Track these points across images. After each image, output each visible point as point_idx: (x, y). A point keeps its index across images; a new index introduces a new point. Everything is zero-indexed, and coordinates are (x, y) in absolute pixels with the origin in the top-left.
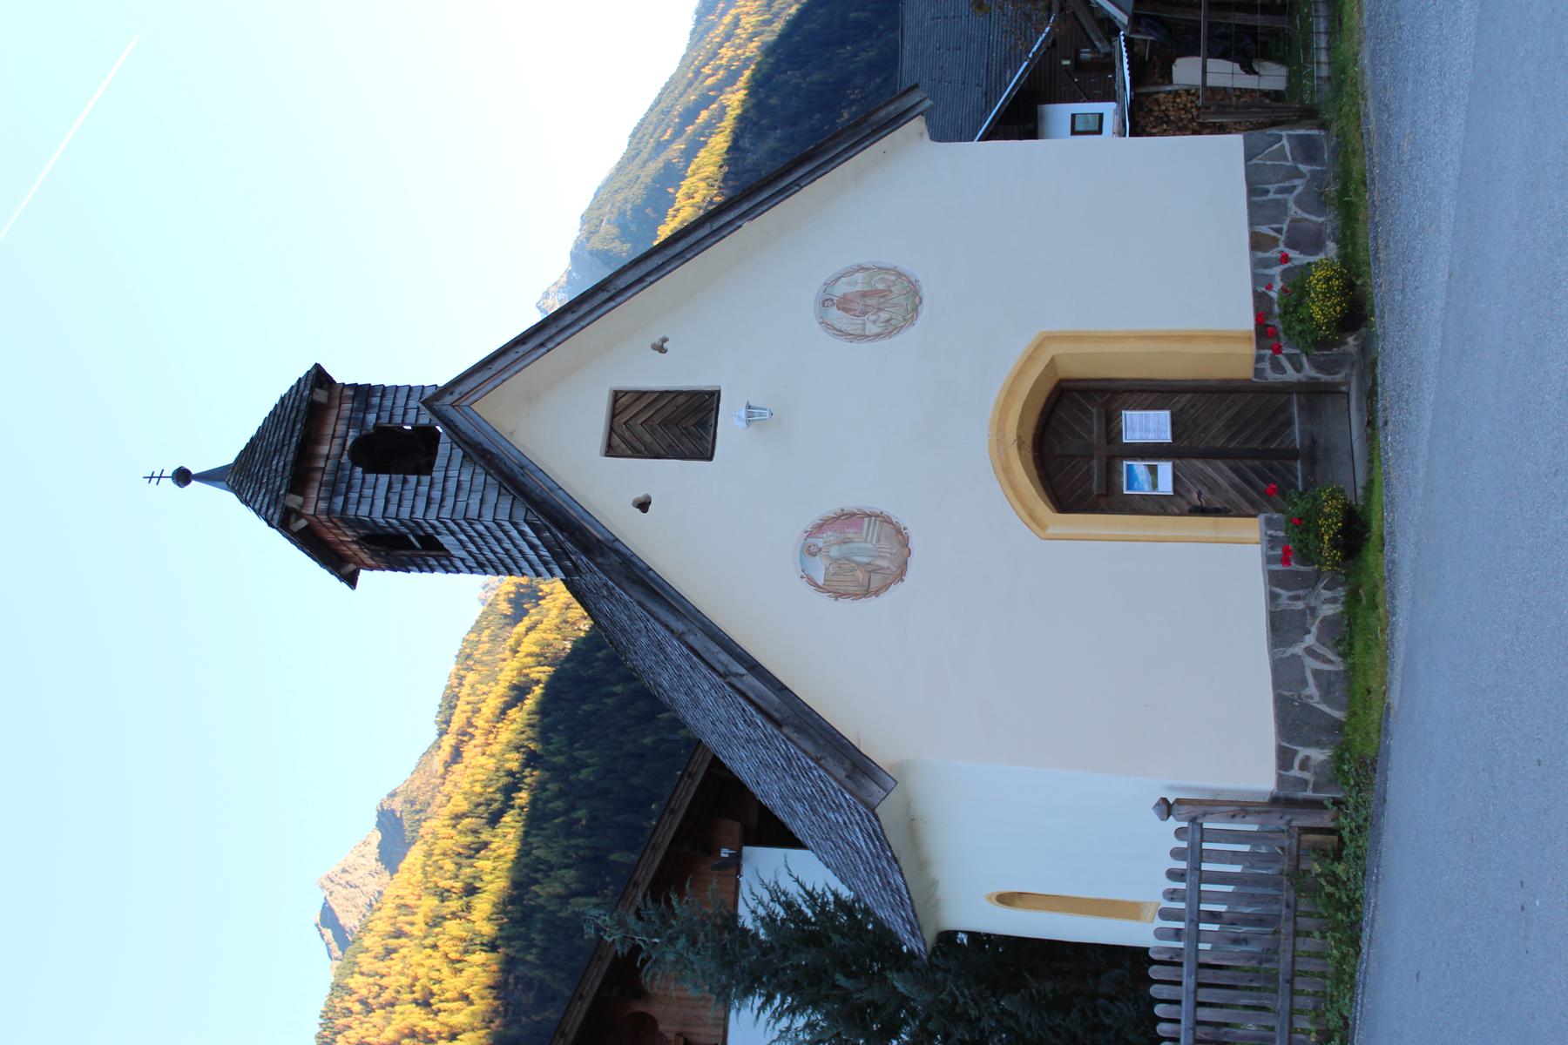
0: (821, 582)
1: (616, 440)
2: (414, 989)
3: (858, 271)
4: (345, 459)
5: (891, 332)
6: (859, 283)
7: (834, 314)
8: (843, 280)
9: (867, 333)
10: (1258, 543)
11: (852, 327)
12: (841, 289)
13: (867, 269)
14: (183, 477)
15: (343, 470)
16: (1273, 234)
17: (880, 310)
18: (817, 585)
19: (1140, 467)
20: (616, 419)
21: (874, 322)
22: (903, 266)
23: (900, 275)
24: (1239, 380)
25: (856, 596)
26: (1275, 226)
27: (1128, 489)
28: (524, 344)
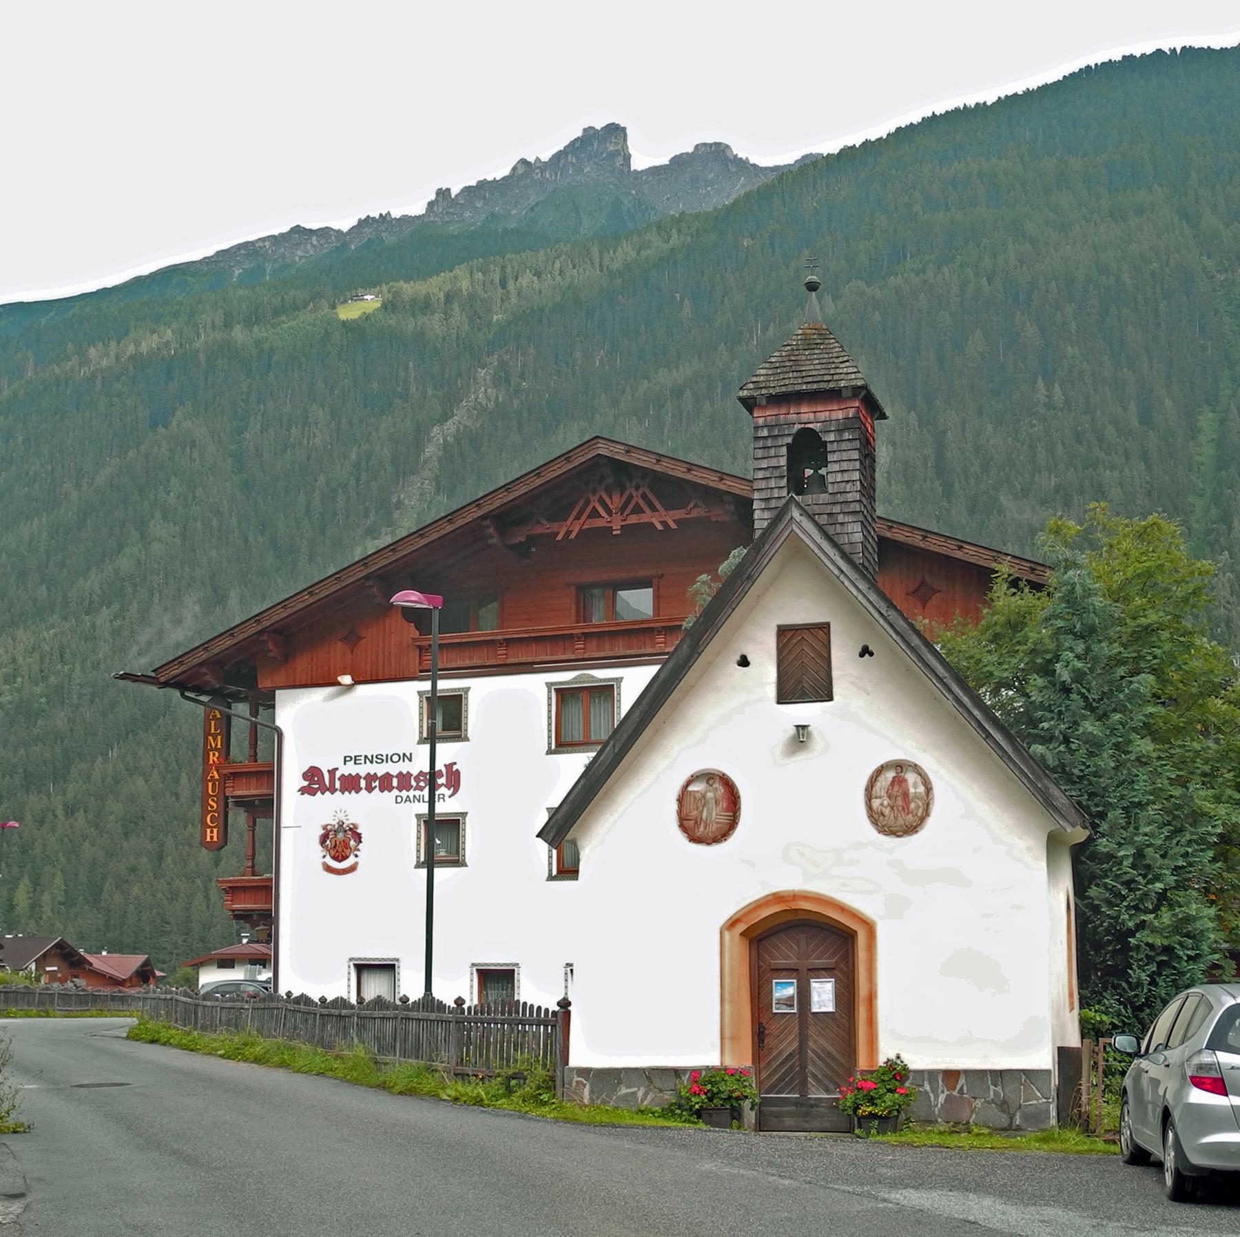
0: (690, 788)
1: (789, 635)
4: (798, 427)
5: (872, 817)
7: (890, 775)
8: (919, 779)
9: (873, 800)
10: (722, 1064)
12: (911, 777)
13: (928, 796)
15: (788, 428)
16: (958, 1087)
17: (892, 808)
19: (791, 991)
20: (806, 631)
24: (206, 968)
25: (680, 812)
26: (965, 1089)
27: (776, 983)
28: (842, 558)
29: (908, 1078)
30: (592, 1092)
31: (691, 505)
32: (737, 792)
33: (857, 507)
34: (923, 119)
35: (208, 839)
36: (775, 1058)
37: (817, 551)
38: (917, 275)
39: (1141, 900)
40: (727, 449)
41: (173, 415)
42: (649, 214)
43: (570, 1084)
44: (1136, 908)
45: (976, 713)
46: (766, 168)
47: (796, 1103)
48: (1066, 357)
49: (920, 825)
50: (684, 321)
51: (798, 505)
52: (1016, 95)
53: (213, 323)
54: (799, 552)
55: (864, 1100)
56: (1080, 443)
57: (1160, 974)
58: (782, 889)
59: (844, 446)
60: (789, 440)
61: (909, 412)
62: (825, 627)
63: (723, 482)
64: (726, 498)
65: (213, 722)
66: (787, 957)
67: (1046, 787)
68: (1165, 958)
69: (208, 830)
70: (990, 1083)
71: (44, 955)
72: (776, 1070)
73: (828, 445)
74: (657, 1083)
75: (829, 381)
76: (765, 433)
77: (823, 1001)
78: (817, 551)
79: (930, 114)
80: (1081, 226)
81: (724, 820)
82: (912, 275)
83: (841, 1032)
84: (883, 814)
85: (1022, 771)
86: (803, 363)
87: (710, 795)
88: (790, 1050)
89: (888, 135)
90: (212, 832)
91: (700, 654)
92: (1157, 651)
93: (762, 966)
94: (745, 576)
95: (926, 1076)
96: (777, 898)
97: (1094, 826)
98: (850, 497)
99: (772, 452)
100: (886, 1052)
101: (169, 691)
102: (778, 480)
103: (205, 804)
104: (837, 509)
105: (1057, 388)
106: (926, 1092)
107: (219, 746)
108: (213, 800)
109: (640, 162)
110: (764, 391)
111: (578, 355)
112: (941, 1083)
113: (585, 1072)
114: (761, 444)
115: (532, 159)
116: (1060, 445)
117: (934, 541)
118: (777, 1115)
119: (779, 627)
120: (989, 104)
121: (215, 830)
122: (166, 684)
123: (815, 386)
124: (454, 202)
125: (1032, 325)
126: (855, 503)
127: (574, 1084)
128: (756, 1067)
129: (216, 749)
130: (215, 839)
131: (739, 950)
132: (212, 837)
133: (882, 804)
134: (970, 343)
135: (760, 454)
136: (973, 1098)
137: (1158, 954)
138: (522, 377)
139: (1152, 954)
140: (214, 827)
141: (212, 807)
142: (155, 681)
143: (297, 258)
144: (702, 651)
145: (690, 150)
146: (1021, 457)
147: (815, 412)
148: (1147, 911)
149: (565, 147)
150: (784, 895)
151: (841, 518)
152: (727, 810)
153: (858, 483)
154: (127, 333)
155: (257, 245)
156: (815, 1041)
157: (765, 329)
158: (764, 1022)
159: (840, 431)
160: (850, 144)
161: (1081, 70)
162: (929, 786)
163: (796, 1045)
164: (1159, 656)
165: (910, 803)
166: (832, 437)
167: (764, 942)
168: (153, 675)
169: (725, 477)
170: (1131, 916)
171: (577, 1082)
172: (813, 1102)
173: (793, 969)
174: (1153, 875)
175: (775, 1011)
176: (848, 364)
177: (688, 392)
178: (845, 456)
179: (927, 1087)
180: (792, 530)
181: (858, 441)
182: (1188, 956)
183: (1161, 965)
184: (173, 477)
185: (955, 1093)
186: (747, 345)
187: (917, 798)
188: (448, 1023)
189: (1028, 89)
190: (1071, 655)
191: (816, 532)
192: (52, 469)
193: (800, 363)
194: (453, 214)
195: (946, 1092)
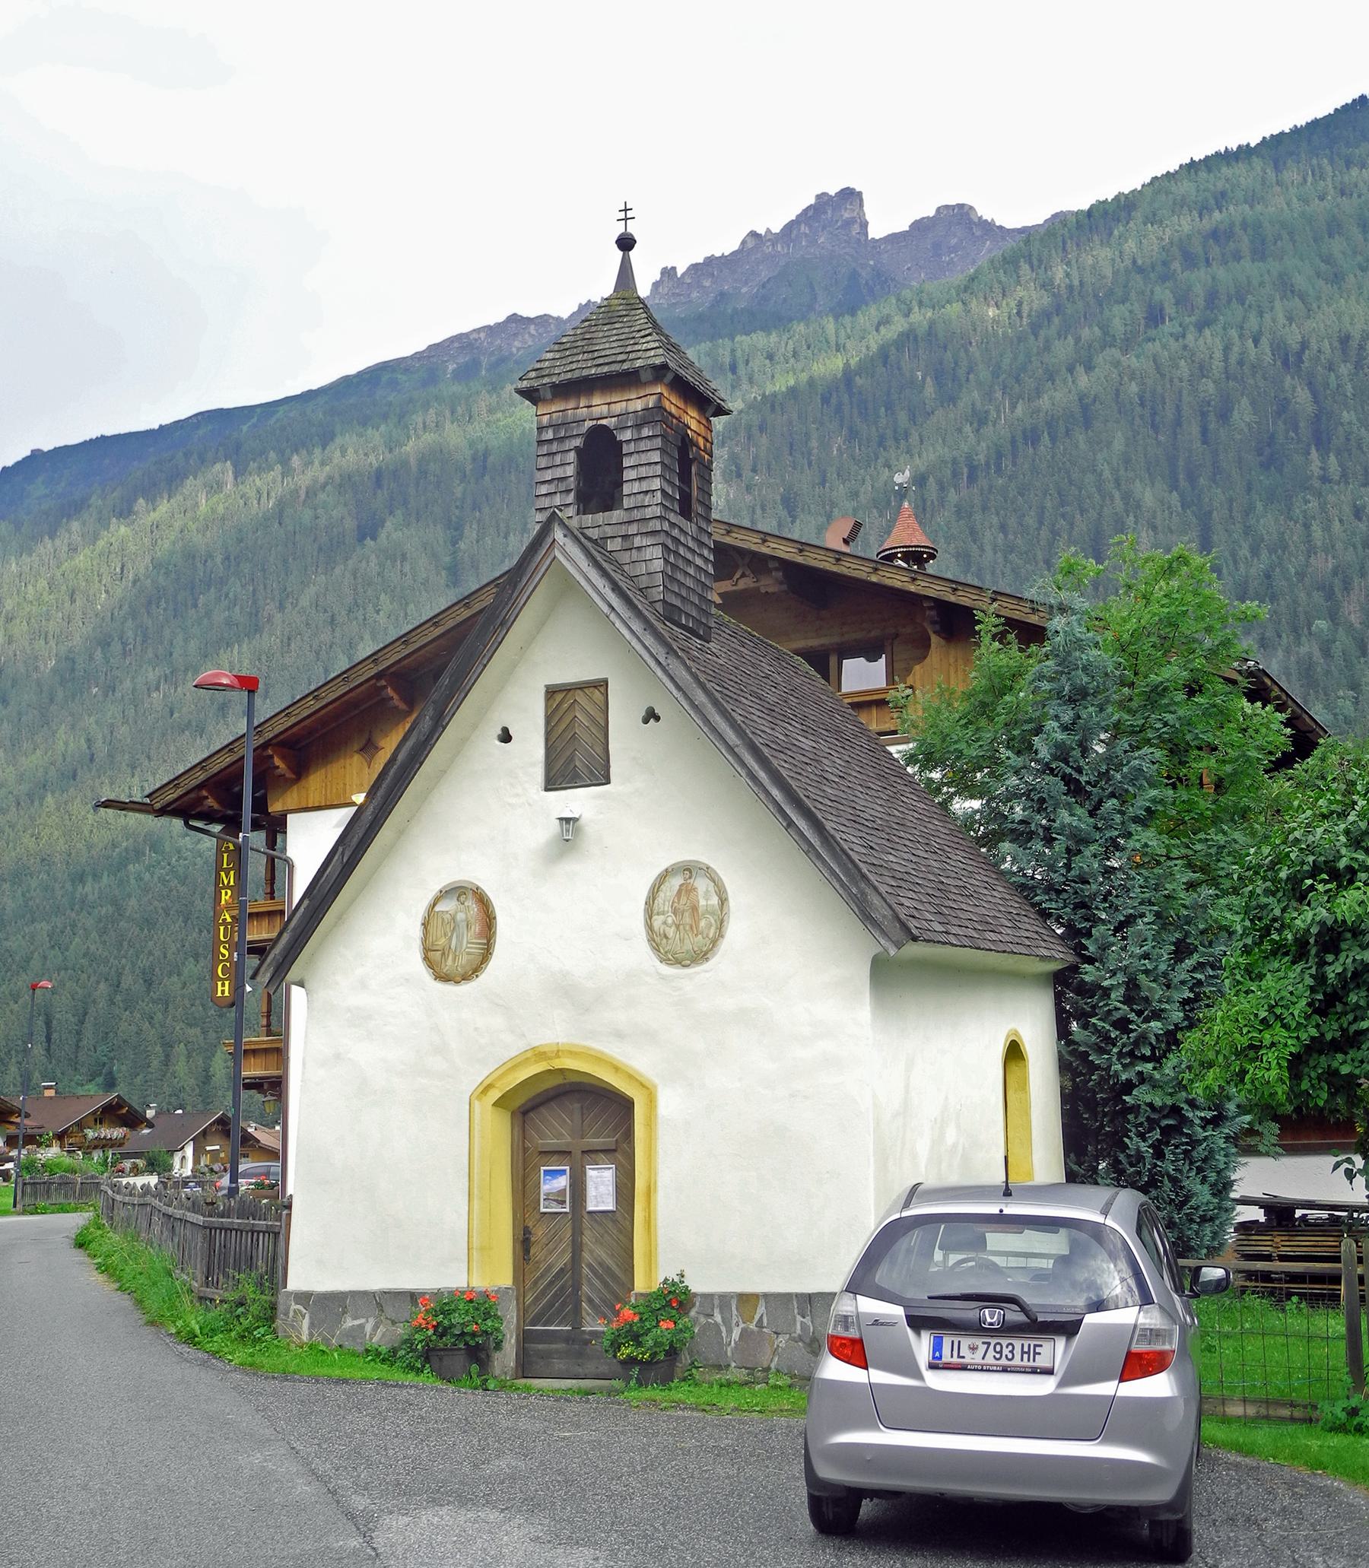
0: (437, 909)
1: (559, 697)
2: (1080, 369)
3: (720, 898)
4: (588, 424)
6: (707, 899)
7: (676, 882)
9: (654, 917)
11: (661, 901)
12: (702, 884)
14: (626, 243)
16: (757, 1317)
17: (678, 927)
18: (434, 905)
19: (562, 1182)
21: (665, 923)
22: (724, 945)
23: (714, 943)
28: (613, 590)
29: (694, 1305)
30: (312, 1325)
31: (737, 575)
32: (493, 911)
33: (656, 525)
34: (1181, 166)
35: (219, 994)
36: (542, 1276)
37: (583, 583)
38: (1177, 340)
39: (1136, 1043)
40: (975, 541)
41: (383, 527)
42: (889, 286)
43: (286, 1314)
44: (1131, 1054)
45: (776, 793)
46: (1013, 230)
47: (567, 1338)
48: (1342, 424)
49: (711, 949)
50: (927, 401)
51: (562, 523)
52: (1282, 134)
53: (424, 423)
54: (568, 586)
55: (626, 1337)
56: (1360, 520)
57: (1167, 1144)
58: (543, 1042)
59: (643, 446)
60: (578, 442)
61: (1171, 492)
62: (602, 685)
63: (766, 544)
64: (772, 565)
65: (225, 855)
66: (559, 1136)
67: (863, 893)
68: (1171, 1122)
69: (220, 983)
70: (796, 1311)
71: (204, 1133)
72: (543, 1293)
73: (624, 445)
74: (389, 1311)
75: (623, 361)
76: (549, 435)
77: (601, 1196)
78: (583, 583)
79: (1188, 161)
80: (1355, 276)
81: (476, 950)
82: (1172, 340)
83: (621, 1237)
84: (666, 937)
85: (833, 872)
86: (598, 341)
87: (460, 916)
88: (560, 1265)
89: (1143, 186)
90: (223, 985)
91: (444, 728)
92: (1168, 717)
93: (529, 1148)
94: (499, 621)
95: (716, 1302)
96: (539, 1054)
97: (1079, 949)
98: (649, 513)
99: (558, 459)
100: (665, 1271)
101: (164, 820)
102: (564, 495)
103: (216, 952)
104: (633, 529)
105: (1332, 458)
106: (716, 1324)
107: (232, 883)
108: (224, 947)
109: (877, 230)
110: (546, 380)
111: (814, 443)
112: (735, 1312)
113: (304, 1297)
114: (545, 449)
115: (762, 231)
116: (1337, 522)
117: (1005, 605)
118: (546, 1356)
119: (547, 687)
120: (1253, 145)
121: (227, 983)
122: (162, 812)
123: (606, 369)
124: (680, 281)
125: (1302, 389)
126: (654, 521)
127: (291, 1314)
128: (518, 1290)
129: (228, 887)
130: (227, 994)
131: (497, 1130)
132: (223, 992)
133: (665, 923)
134: (1236, 412)
135: (543, 462)
136: (775, 1333)
137: (1165, 1117)
138: (754, 470)
139: (1155, 1116)
140: (226, 979)
141: (224, 955)
142: (149, 808)
143: (514, 350)
144: (447, 724)
145: (931, 213)
146: (1295, 538)
147: (609, 404)
148: (1145, 1059)
149: (798, 216)
150: (546, 1049)
151: (638, 541)
152: (480, 935)
153: (659, 493)
154: (332, 439)
155: (471, 337)
156: (591, 1252)
157: (1013, 407)
158: (530, 1224)
159: (638, 426)
160: (1102, 199)
161: (1354, 100)
162: (724, 896)
163: (567, 1257)
164: (1171, 723)
165: (700, 920)
166: (627, 435)
167: (532, 1114)
168: (148, 801)
169: (768, 538)
170: (1124, 1066)
171: (295, 1311)
172: (587, 1337)
173: (565, 1152)
174: (1152, 1011)
175: (543, 1210)
176: (649, 338)
177: (931, 479)
178: (644, 458)
179: (718, 1318)
180: (555, 557)
181: (660, 439)
182: (1201, 1118)
183: (1166, 1131)
184: (383, 595)
185: (752, 1326)
186: (994, 426)
187: (709, 913)
188: (234, 1232)
189: (1296, 126)
190: (1055, 724)
191: (583, 557)
192: (254, 590)
193: (595, 341)
194: (679, 295)
195: (742, 1325)
